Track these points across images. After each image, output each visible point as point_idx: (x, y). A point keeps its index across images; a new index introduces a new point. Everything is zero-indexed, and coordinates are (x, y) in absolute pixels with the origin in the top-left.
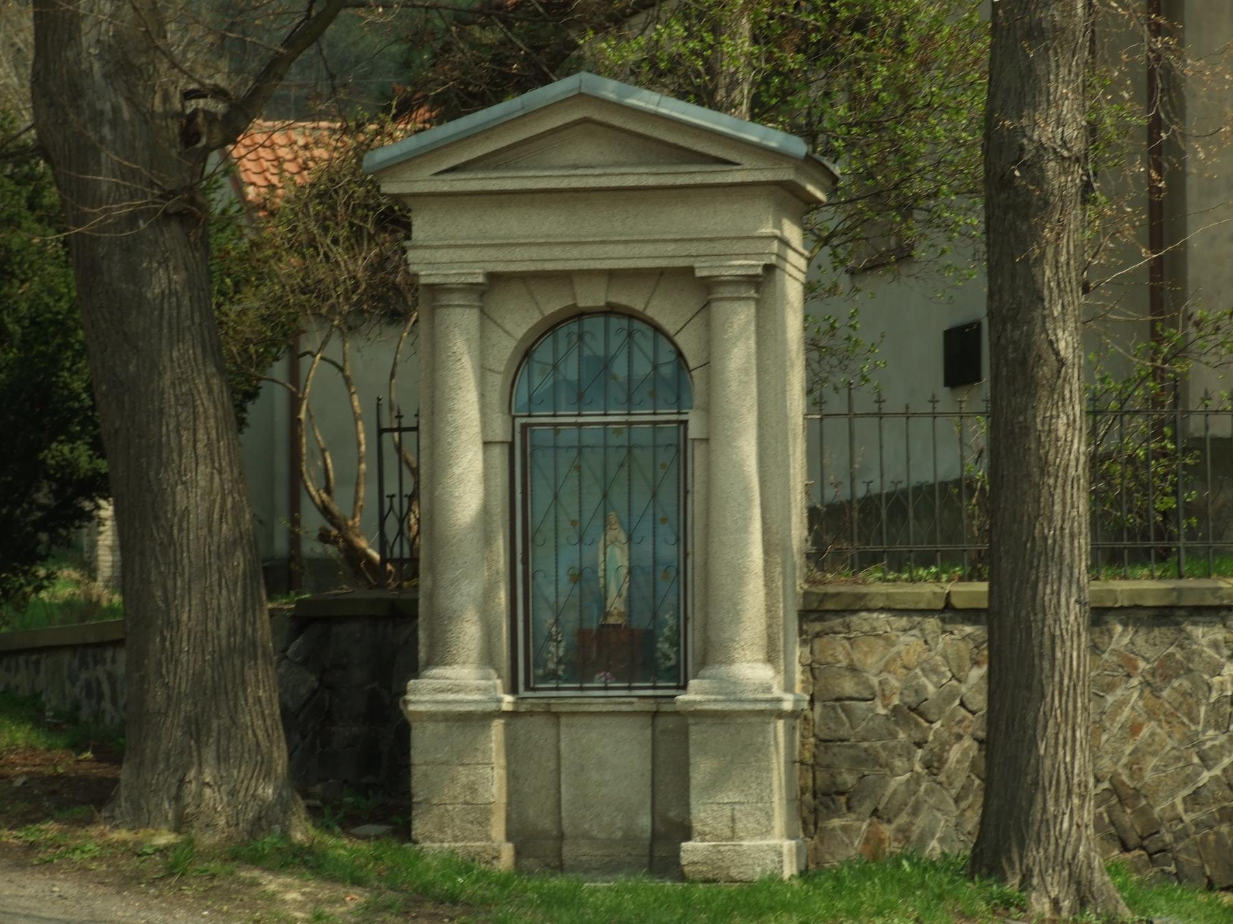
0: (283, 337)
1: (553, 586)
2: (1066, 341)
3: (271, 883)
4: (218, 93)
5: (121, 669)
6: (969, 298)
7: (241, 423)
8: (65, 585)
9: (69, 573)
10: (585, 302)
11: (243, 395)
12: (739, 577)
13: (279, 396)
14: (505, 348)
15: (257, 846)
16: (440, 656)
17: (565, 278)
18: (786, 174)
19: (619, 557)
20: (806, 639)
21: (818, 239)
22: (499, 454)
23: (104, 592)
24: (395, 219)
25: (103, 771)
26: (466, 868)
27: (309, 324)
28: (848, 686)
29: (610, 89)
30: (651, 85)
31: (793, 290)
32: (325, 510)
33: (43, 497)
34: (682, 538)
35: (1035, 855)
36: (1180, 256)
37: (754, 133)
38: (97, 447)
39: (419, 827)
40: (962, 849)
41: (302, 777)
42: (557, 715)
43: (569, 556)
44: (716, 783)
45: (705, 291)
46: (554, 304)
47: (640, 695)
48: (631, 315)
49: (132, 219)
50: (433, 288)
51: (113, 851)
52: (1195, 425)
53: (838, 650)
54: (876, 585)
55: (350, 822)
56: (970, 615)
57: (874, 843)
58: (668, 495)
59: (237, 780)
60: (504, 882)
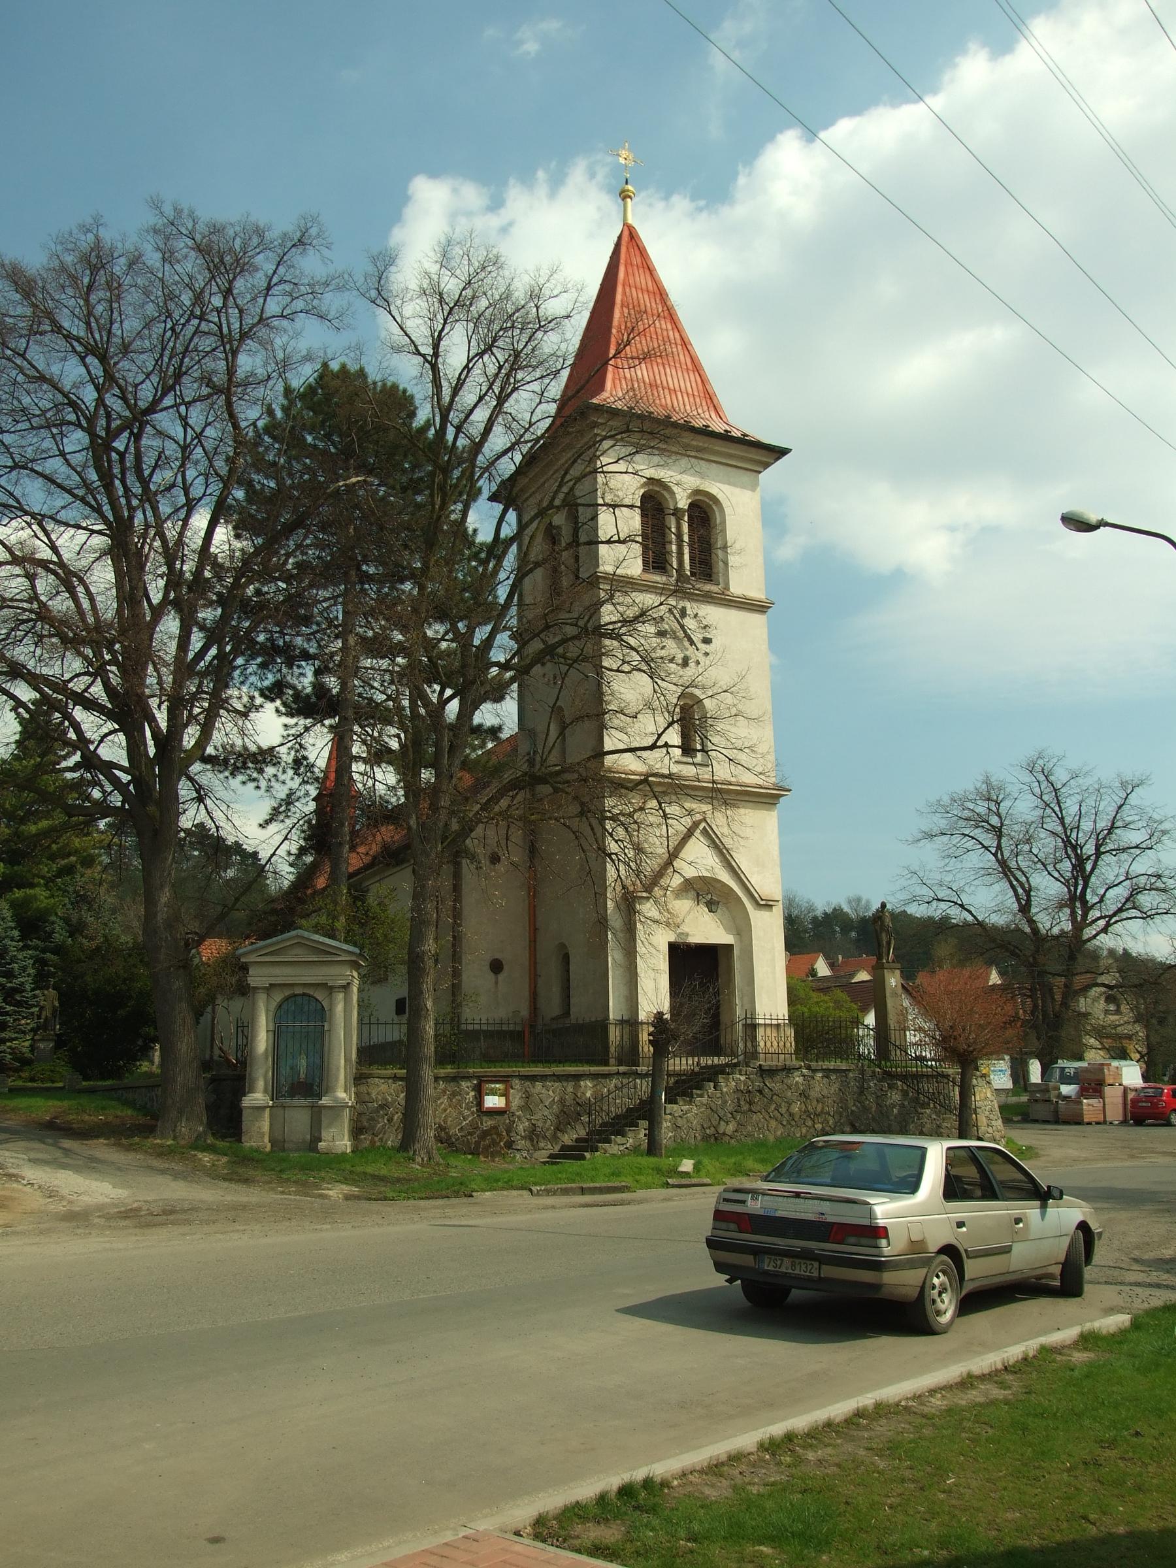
0: (211, 999)
1: (285, 1071)
2: (429, 1005)
3: (200, 1155)
4: (196, 933)
5: (159, 1093)
6: (404, 992)
7: (198, 1023)
8: (145, 1067)
9: (147, 1063)
10: (297, 992)
11: (198, 1014)
12: (338, 1069)
13: (209, 1017)
14: (274, 1005)
15: (198, 1144)
16: (252, 1090)
17: (292, 985)
18: (354, 958)
19: (303, 1063)
20: (356, 1085)
21: (361, 977)
22: (271, 1034)
23: (155, 1069)
24: (244, 968)
25: (153, 1122)
26: (256, 1151)
27: (219, 996)
28: (367, 1099)
29: (306, 934)
30: (316, 933)
31: (355, 990)
32: (221, 1049)
33: (140, 1042)
34: (322, 1057)
35: (417, 1146)
36: (460, 981)
37: (345, 947)
38: (156, 1029)
39: (243, 1139)
40: (397, 1144)
41: (210, 1125)
42: (332, 988)
43: (290, 1062)
44: (329, 1126)
45: (330, 990)
46: (287, 993)
47: (307, 1102)
48: (309, 996)
49: (169, 968)
50: (255, 988)
51: (154, 1146)
52: (463, 1027)
53: (363, 1089)
54: (375, 1070)
55: (223, 1137)
56: (401, 1079)
57: (373, 1142)
58: (318, 1046)
59: (190, 1127)
60: (268, 1154)
